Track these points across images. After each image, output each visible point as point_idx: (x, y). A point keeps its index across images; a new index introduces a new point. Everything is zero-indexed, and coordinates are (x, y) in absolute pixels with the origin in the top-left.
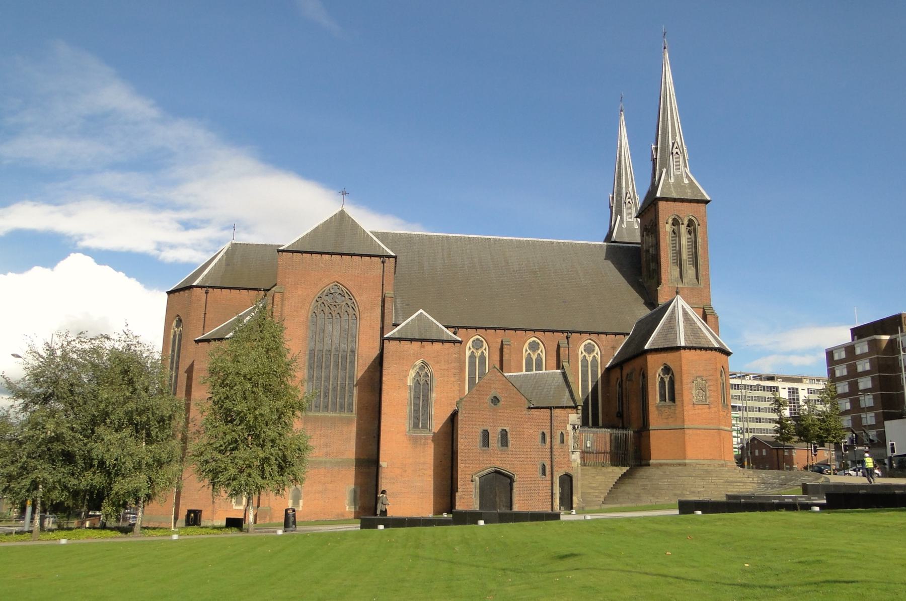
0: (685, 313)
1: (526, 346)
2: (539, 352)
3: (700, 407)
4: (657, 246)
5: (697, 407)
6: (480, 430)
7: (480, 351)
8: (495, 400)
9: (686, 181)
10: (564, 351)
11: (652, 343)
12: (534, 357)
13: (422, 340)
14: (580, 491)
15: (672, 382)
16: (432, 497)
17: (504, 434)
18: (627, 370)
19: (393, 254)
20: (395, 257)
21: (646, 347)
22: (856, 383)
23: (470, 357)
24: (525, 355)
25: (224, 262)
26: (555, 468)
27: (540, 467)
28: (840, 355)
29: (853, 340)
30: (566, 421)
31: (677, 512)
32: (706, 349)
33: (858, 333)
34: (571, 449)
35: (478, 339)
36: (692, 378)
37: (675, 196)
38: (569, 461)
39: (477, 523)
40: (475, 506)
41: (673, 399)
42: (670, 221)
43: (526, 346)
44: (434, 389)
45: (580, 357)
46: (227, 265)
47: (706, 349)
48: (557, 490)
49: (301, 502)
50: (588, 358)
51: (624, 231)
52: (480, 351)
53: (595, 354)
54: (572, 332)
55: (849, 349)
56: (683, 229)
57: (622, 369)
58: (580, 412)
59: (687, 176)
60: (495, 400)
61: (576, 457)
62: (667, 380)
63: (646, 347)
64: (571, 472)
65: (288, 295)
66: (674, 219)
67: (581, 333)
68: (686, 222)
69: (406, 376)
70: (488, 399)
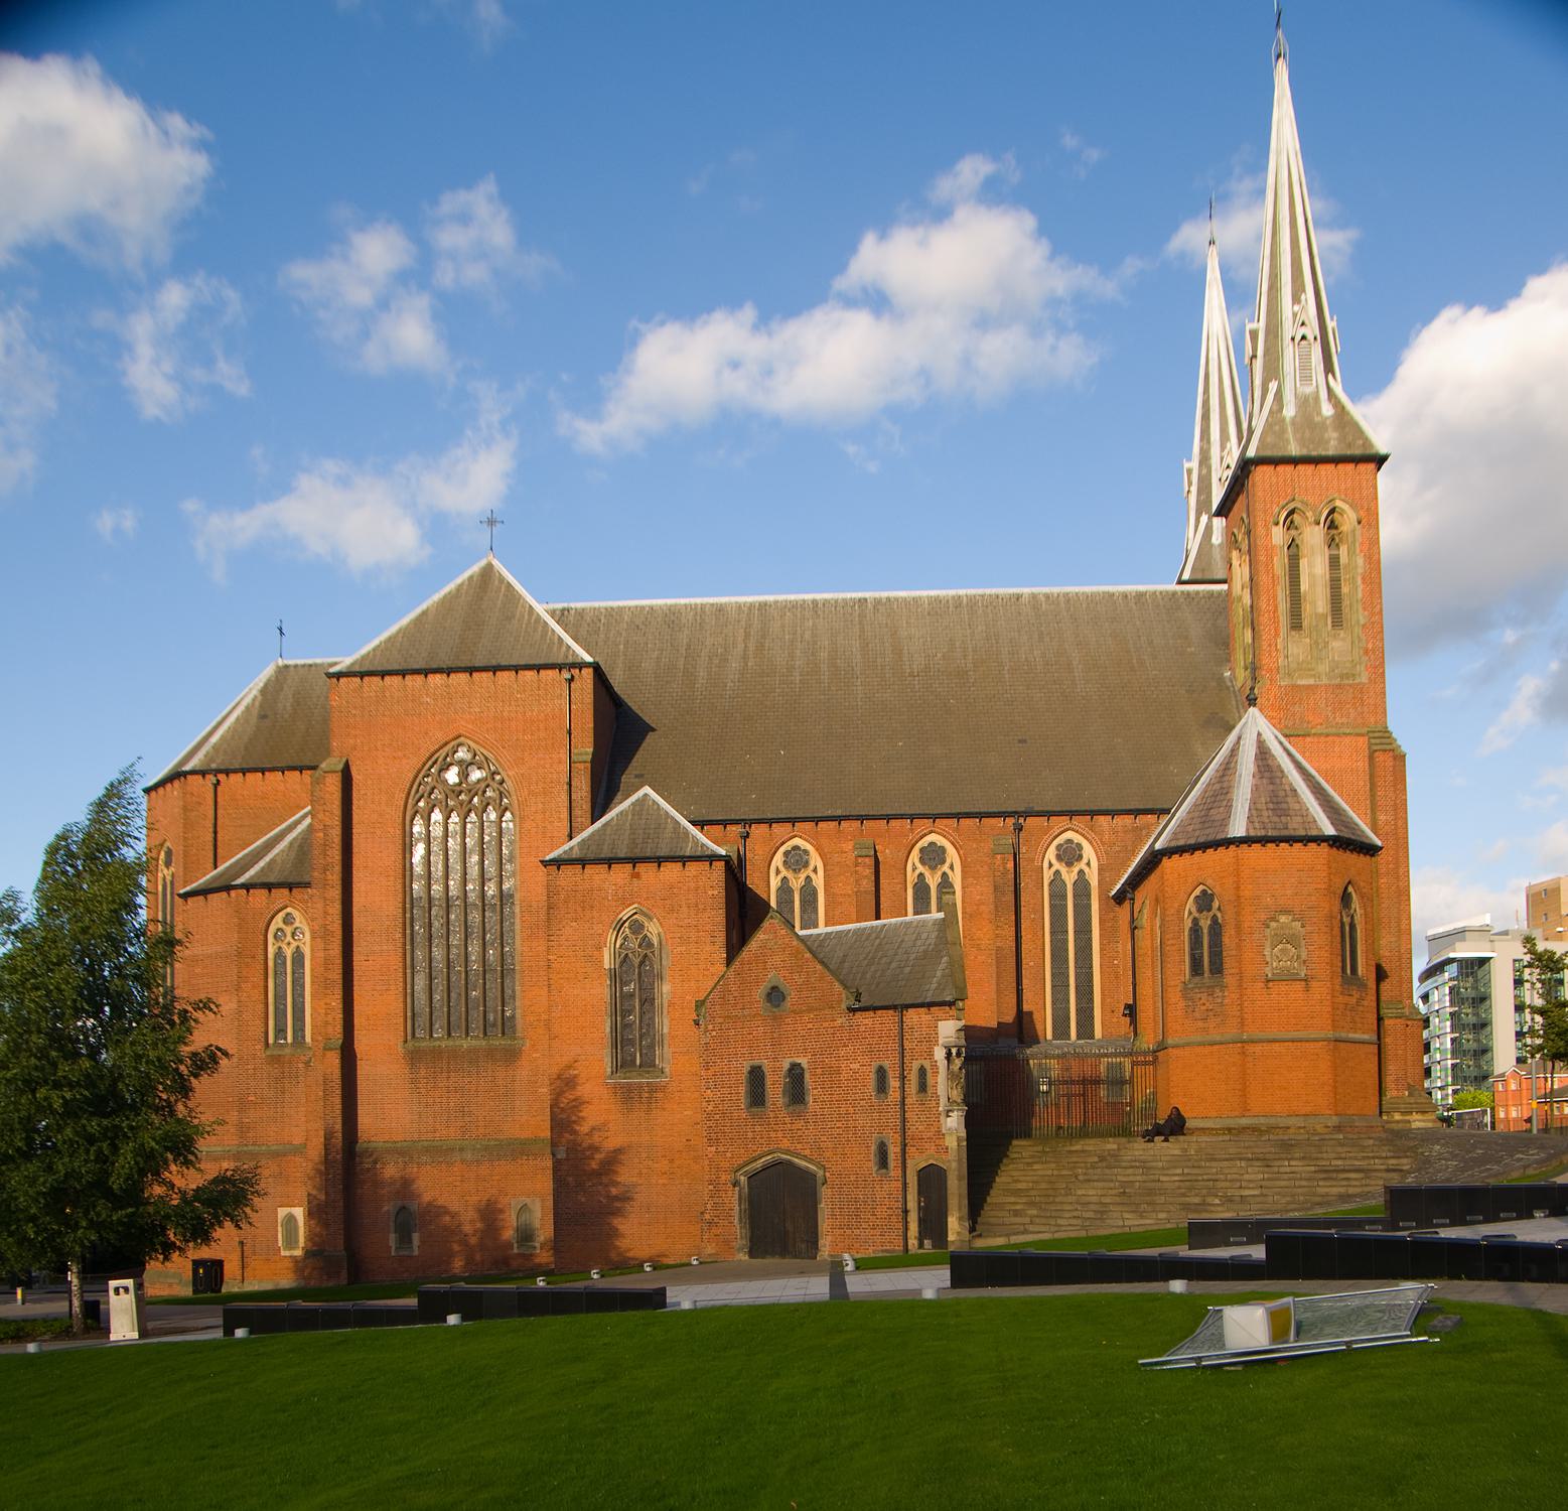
0: (1263, 753)
1: (915, 855)
2: (946, 868)
3: (1283, 987)
5: (1275, 987)
7: (802, 876)
9: (1327, 410)
17: (796, 1074)
19: (589, 659)
24: (911, 878)
25: (255, 712)
30: (931, 1040)
34: (943, 1101)
36: (1263, 917)
37: (1294, 450)
38: (940, 1135)
41: (1217, 968)
43: (915, 855)
44: (666, 973)
45: (1048, 875)
46: (263, 717)
47: (1307, 840)
48: (912, 1205)
49: (416, 1237)
50: (1065, 876)
52: (802, 876)
60: (775, 995)
62: (1205, 924)
67: (1049, 814)
69: (599, 948)
70: (760, 992)
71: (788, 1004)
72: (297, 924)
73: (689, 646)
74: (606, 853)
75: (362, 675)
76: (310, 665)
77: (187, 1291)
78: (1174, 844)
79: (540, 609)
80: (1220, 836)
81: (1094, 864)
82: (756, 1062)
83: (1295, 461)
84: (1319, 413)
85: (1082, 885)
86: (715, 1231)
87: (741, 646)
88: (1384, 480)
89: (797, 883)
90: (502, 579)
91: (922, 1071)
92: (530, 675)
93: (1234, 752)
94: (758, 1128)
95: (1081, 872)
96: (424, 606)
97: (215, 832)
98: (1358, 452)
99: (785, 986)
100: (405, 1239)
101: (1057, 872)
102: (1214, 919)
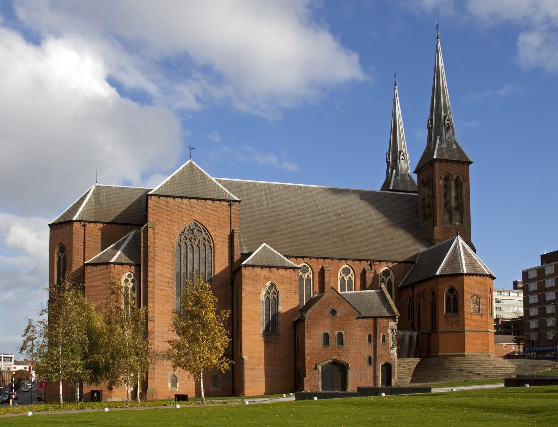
1: (340, 271)
2: (350, 275)
3: (476, 316)
4: (433, 196)
5: (474, 316)
6: (322, 334)
7: (306, 275)
8: (333, 312)
9: (455, 147)
11: (442, 271)
12: (347, 279)
13: (270, 267)
14: (396, 374)
15: (456, 299)
16: (243, 331)
17: (340, 335)
18: (418, 289)
19: (238, 199)
20: (239, 202)
21: (437, 273)
22: (544, 296)
24: (339, 278)
25: (93, 201)
26: (379, 359)
27: (367, 358)
28: (533, 275)
29: (542, 264)
30: (386, 327)
31: (502, 385)
32: (480, 275)
33: (545, 258)
36: (470, 296)
38: (389, 354)
39: (380, 395)
43: (340, 271)
44: (280, 303)
46: (97, 204)
47: (480, 275)
48: (380, 374)
49: (178, 385)
51: (399, 181)
52: (306, 275)
53: (390, 277)
54: (374, 261)
55: (540, 271)
58: (397, 320)
60: (333, 312)
61: (394, 351)
62: (452, 297)
63: (437, 273)
64: (390, 362)
65: (157, 230)
66: (446, 176)
68: (455, 177)
69: (259, 294)
70: (327, 312)
71: (338, 314)
72: (127, 277)
75: (159, 196)
76: (108, 187)
78: (443, 274)
79: (213, 179)
81: (393, 277)
82: (326, 332)
84: (452, 147)
85: (308, 279)
86: (309, 382)
88: (470, 166)
91: (384, 336)
92: (186, 200)
93: (455, 248)
94: (326, 352)
95: (390, 279)
97: (84, 243)
99: (335, 309)
101: (383, 279)
102: (455, 296)
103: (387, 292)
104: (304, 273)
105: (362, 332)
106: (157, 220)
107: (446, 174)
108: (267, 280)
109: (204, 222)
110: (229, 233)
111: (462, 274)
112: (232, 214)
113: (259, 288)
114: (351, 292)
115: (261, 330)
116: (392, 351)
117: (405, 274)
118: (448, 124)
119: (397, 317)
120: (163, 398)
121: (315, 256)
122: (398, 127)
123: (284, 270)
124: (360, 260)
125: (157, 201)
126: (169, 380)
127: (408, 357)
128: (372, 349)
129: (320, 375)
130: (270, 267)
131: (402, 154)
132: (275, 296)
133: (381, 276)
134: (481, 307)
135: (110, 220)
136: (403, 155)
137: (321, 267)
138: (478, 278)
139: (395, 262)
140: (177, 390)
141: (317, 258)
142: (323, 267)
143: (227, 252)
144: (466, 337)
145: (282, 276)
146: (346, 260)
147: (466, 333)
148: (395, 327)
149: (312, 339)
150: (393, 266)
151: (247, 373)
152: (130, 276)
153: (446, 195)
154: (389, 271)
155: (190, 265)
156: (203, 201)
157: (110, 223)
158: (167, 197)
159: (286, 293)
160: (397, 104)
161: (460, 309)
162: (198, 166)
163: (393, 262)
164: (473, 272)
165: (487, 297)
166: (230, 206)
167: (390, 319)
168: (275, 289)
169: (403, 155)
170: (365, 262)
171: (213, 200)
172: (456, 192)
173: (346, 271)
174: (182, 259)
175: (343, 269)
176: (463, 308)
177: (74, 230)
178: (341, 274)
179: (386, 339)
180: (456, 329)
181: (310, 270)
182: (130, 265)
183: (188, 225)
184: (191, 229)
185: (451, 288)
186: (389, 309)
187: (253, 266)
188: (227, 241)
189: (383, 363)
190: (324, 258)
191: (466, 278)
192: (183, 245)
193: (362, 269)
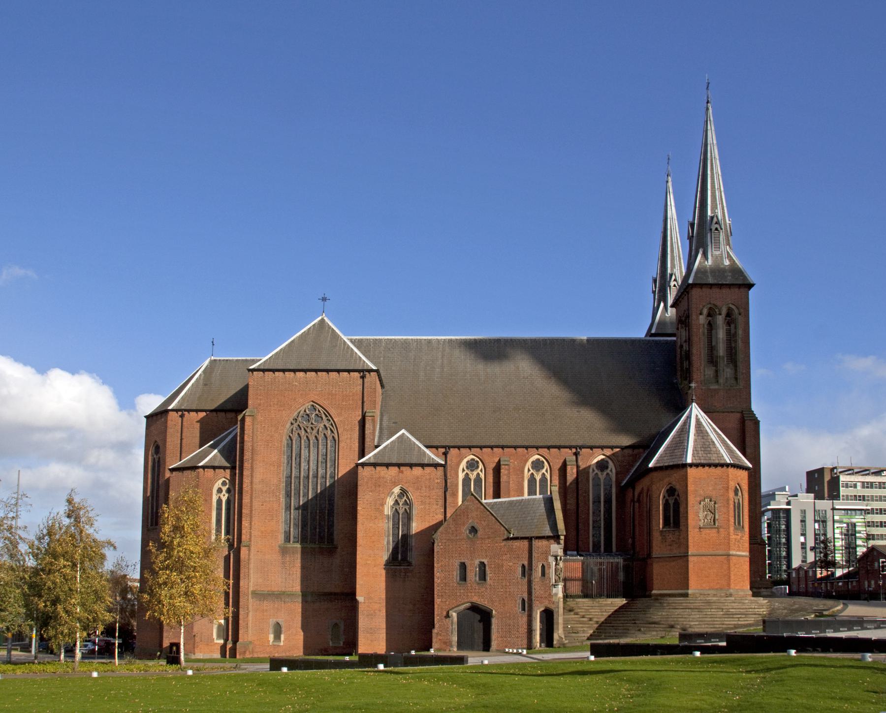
1: (529, 464)
2: (544, 471)
3: (708, 531)
5: (704, 531)
7: (475, 473)
8: (474, 530)
10: (572, 469)
11: (658, 461)
12: (538, 477)
13: (399, 465)
15: (677, 504)
19: (374, 368)
20: (377, 371)
21: (650, 465)
23: (464, 480)
24: (527, 475)
25: (201, 382)
30: (547, 553)
35: (473, 460)
36: (699, 499)
40: (380, 648)
41: (677, 524)
42: (705, 311)
43: (529, 464)
44: (414, 518)
49: (282, 637)
52: (475, 473)
54: (581, 447)
56: (720, 320)
57: (634, 489)
58: (562, 542)
59: (729, 256)
60: (474, 530)
62: (671, 502)
63: (650, 465)
64: (552, 607)
65: (260, 418)
68: (724, 311)
69: (383, 505)
70: (465, 530)
71: (479, 533)
73: (415, 359)
74: (386, 461)
75: (264, 371)
77: (297, 652)
78: (658, 465)
79: (345, 338)
80: (680, 463)
81: (614, 471)
82: (463, 561)
83: (711, 286)
87: (440, 361)
88: (752, 292)
89: (473, 476)
90: (330, 327)
91: (543, 566)
92: (301, 374)
93: (685, 423)
95: (608, 474)
96: (292, 339)
97: (181, 439)
98: (740, 282)
100: (277, 637)
102: (676, 499)
103: (558, 498)
104: (472, 471)
105: (512, 561)
106: (260, 405)
107: (709, 306)
108: (395, 484)
109: (325, 403)
110: (360, 417)
111: (685, 466)
112: (365, 390)
113: (382, 496)
114: (534, 497)
115: (385, 556)
116: (554, 590)
117: (633, 466)
118: (716, 229)
119: (562, 537)
120: (262, 656)
121: (488, 444)
122: (669, 238)
123: (420, 468)
124: (559, 447)
125: (261, 378)
126: (271, 630)
127: (608, 596)
128: (525, 588)
129: (455, 626)
130: (399, 465)
131: (673, 278)
132: (407, 507)
133: (593, 470)
134: (717, 517)
135: (213, 407)
136: (675, 280)
137: (496, 460)
138: (713, 469)
139: (617, 447)
140: (282, 644)
141: (492, 447)
142: (499, 461)
143: (357, 445)
144: (691, 566)
145: (418, 478)
146: (537, 448)
147: (691, 559)
148: (560, 552)
149: (444, 573)
150: (613, 454)
151: (363, 622)
152: (224, 484)
153: (731, 337)
154: (607, 462)
155: (304, 465)
156: (324, 373)
157: (215, 411)
158: (274, 371)
159: (422, 503)
160: (669, 203)
161: (682, 520)
162: (331, 324)
163: (612, 448)
164: (702, 462)
165: (728, 500)
166: (363, 377)
167: (552, 541)
168: (408, 497)
169: (675, 280)
170: (567, 450)
171: (338, 371)
172: (728, 332)
173: (537, 465)
174: (293, 457)
175: (533, 463)
176: (687, 519)
177: (169, 423)
178: (529, 470)
179: (547, 571)
180: (676, 552)
181: (481, 466)
182: (224, 468)
183: (302, 409)
184: (308, 415)
185: (671, 487)
186: (554, 526)
187: (375, 465)
188: (357, 428)
189: (543, 609)
190: (503, 447)
191: (691, 471)
192: (295, 437)
193: (562, 461)
